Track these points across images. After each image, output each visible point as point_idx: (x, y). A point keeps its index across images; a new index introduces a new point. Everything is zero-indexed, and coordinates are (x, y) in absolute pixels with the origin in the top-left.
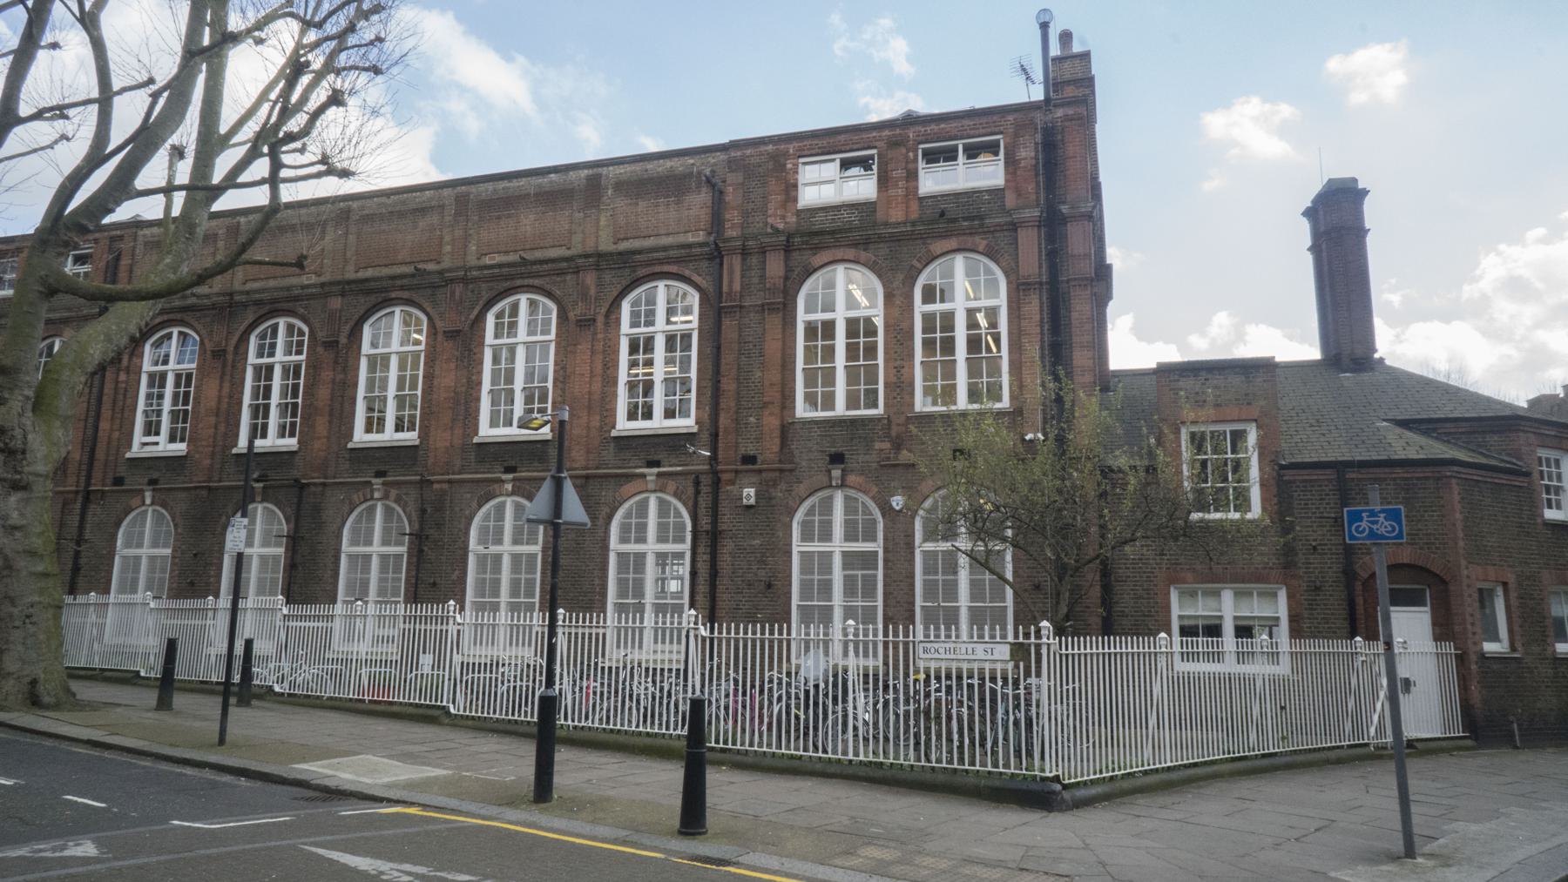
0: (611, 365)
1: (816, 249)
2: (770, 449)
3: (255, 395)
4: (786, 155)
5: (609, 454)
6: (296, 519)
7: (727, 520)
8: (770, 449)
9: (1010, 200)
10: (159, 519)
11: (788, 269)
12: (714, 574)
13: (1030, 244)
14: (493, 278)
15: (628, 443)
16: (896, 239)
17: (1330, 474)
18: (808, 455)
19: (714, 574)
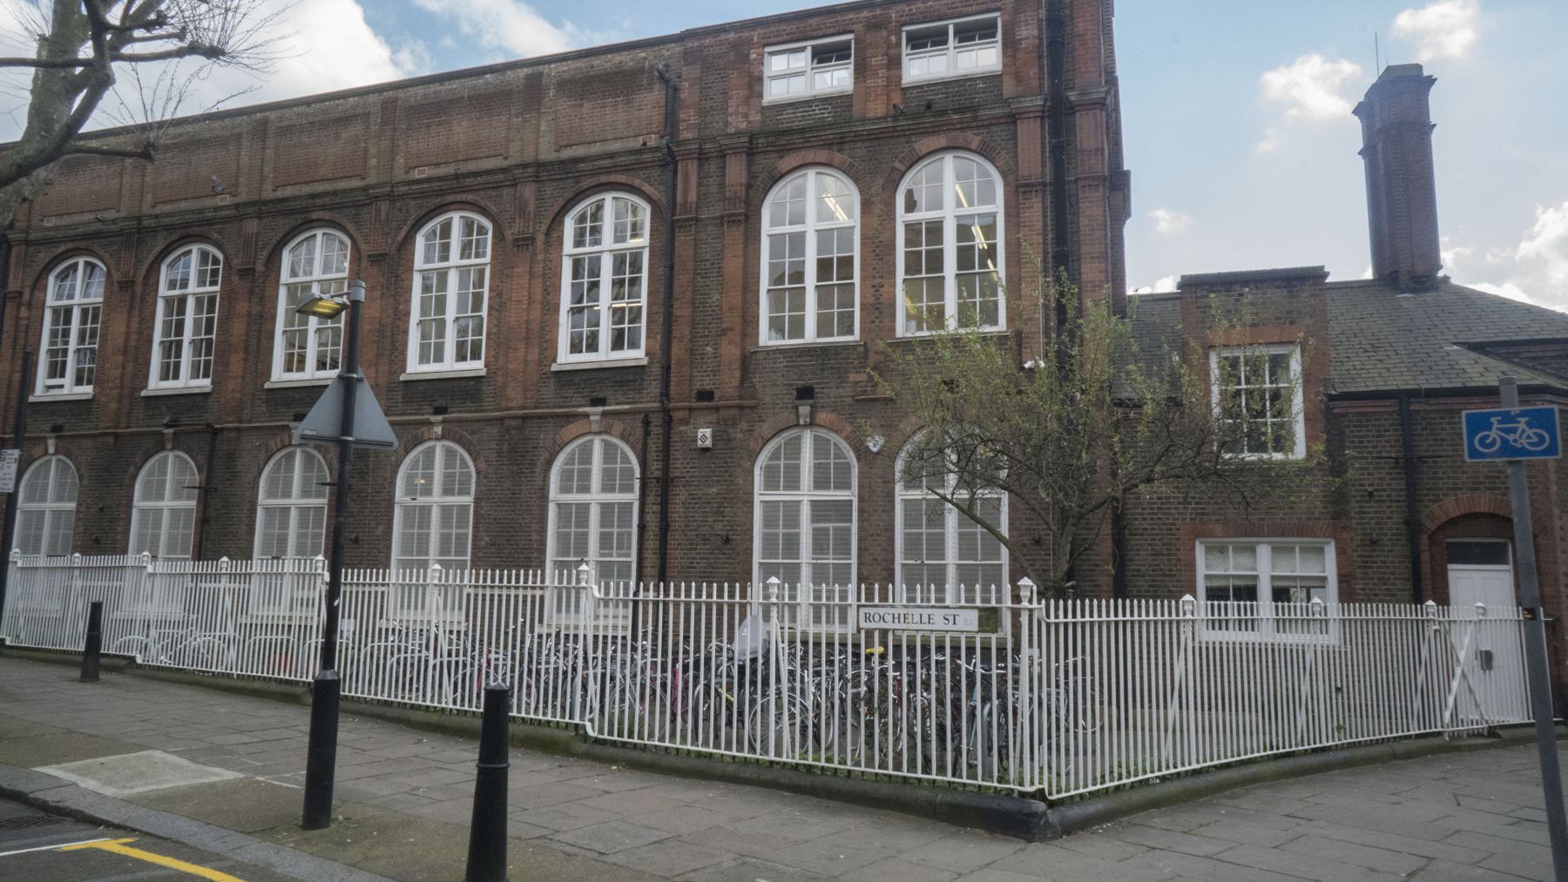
0: (553, 289)
1: (783, 151)
2: (728, 383)
3: (166, 332)
4: (749, 43)
5: (549, 391)
6: (208, 469)
7: (679, 467)
8: (728, 383)
9: (1009, 88)
10: (63, 469)
11: (752, 176)
12: (665, 527)
13: (1031, 139)
14: (423, 195)
15: (569, 377)
16: (875, 137)
17: (1390, 406)
18: (772, 389)
19: (665, 527)
